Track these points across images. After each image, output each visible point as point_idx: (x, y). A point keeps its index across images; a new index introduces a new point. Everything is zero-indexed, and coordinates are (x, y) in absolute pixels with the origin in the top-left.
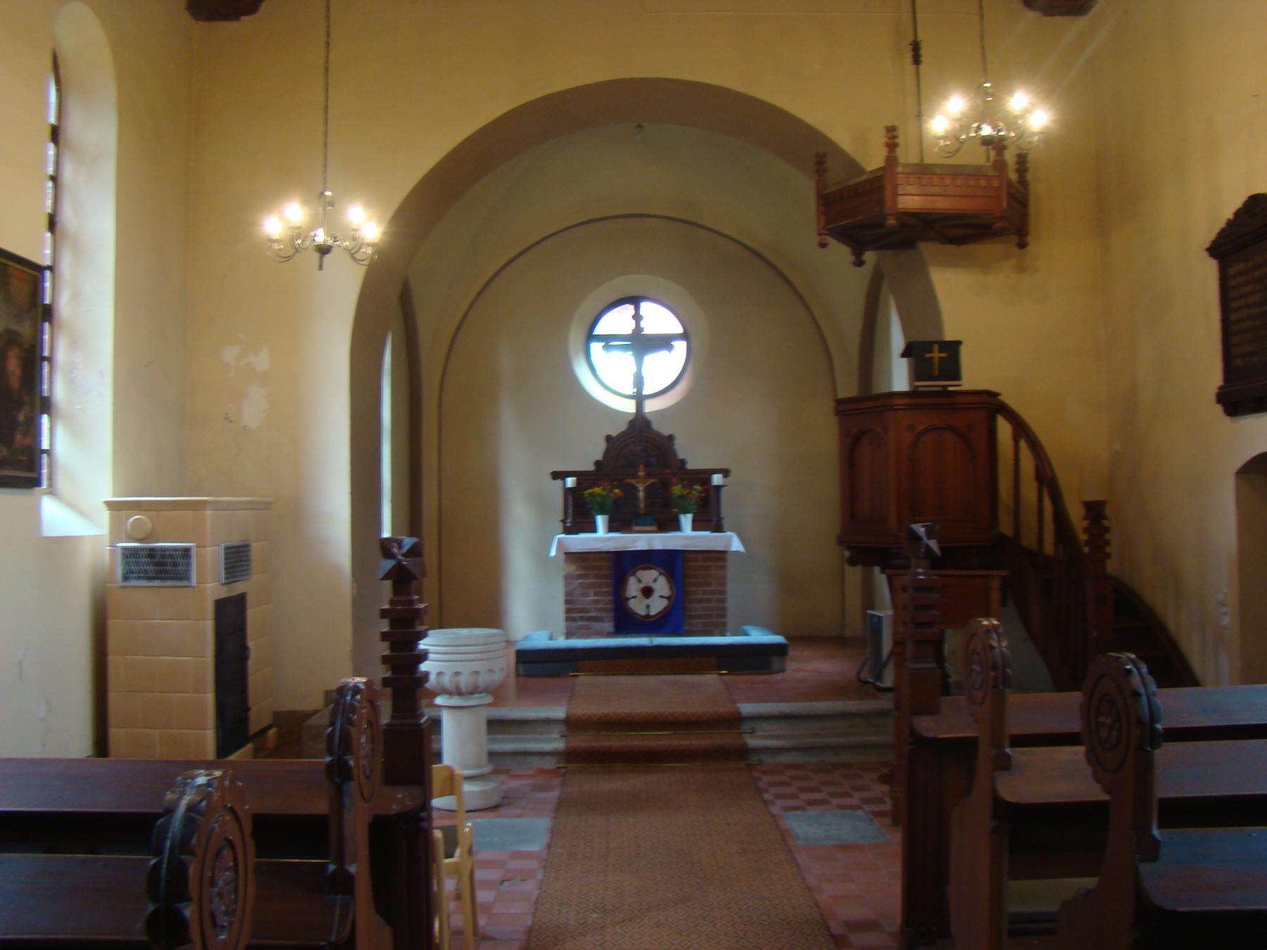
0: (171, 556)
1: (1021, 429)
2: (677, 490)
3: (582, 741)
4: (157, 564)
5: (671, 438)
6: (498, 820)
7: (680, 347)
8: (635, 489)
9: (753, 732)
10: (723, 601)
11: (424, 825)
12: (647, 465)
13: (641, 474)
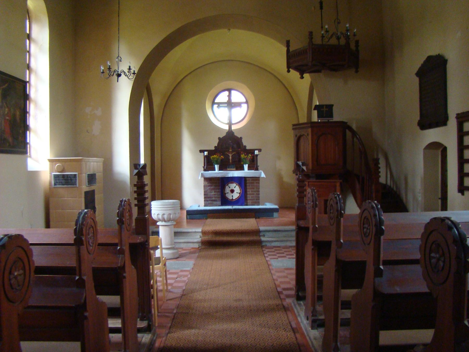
0: (70, 177)
1: (354, 133)
2: (243, 156)
3: (207, 238)
4: (65, 180)
5: (241, 138)
6: (177, 262)
7: (245, 106)
8: (229, 156)
9: (264, 236)
10: (259, 194)
11: (147, 246)
12: (232, 148)
13: (231, 150)
